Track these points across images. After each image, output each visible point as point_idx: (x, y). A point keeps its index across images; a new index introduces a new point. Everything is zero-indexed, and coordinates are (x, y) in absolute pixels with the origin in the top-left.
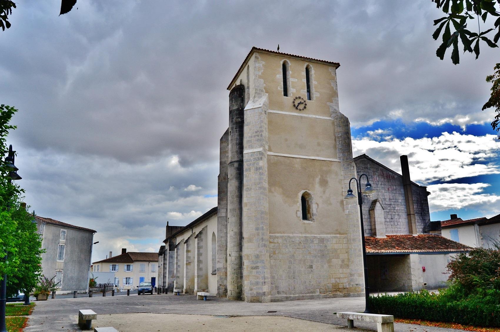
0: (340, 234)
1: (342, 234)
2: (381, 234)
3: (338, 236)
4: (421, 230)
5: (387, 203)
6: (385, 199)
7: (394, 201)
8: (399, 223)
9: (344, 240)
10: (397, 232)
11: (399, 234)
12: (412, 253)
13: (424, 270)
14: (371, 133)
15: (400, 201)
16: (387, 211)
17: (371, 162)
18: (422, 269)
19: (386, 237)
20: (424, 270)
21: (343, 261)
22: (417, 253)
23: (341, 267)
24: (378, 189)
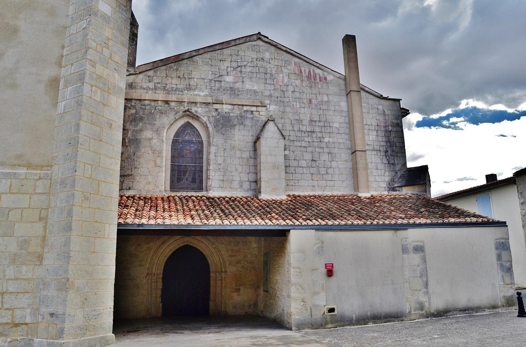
0: (29, 166)
1: (36, 167)
2: (274, 190)
3: (22, 171)
4: (384, 185)
5: (304, 129)
6: (300, 121)
7: (322, 124)
8: (330, 171)
9: (40, 183)
10: (324, 188)
11: (335, 193)
12: (295, 227)
13: (330, 273)
14: (445, 123)
15: (336, 125)
16: (304, 144)
17: (273, 49)
18: (324, 271)
19: (286, 197)
20: (330, 273)
21: (24, 243)
22: (307, 227)
23: (15, 259)
24: (286, 100)
